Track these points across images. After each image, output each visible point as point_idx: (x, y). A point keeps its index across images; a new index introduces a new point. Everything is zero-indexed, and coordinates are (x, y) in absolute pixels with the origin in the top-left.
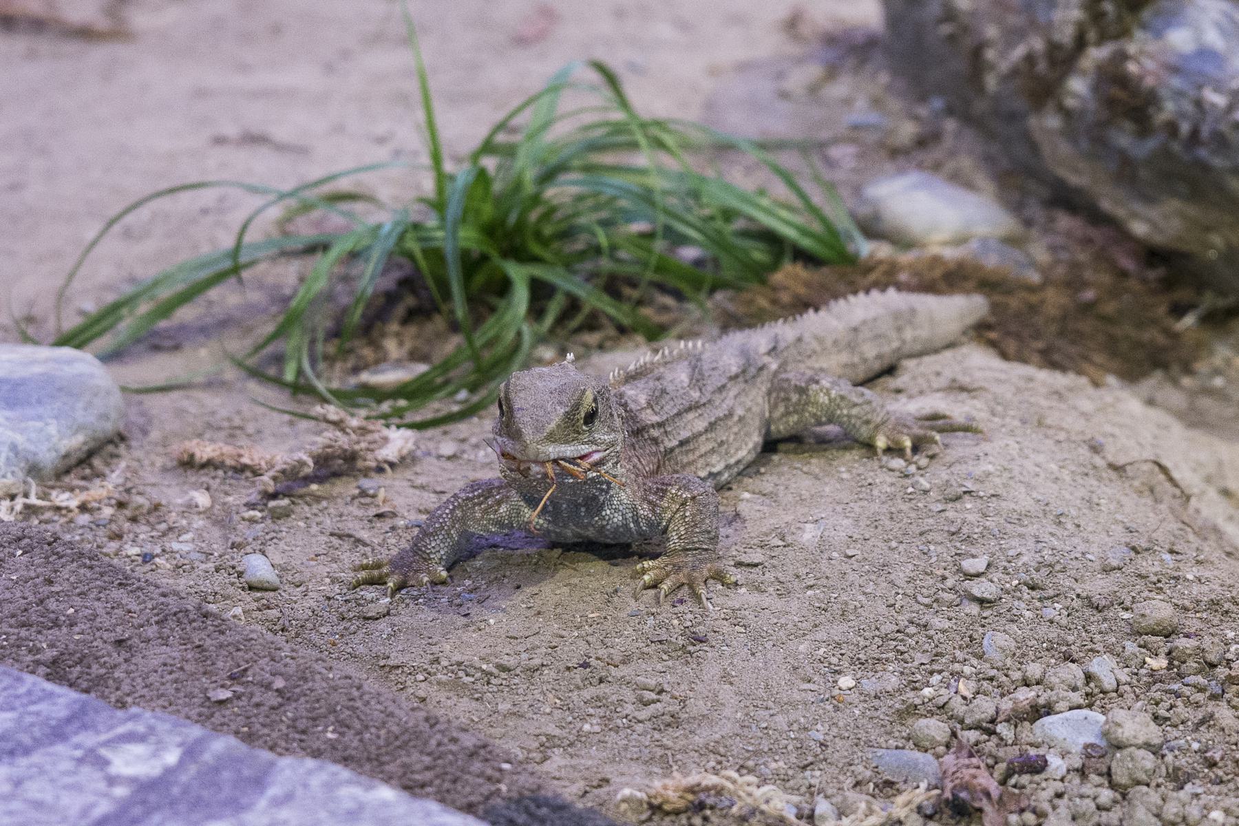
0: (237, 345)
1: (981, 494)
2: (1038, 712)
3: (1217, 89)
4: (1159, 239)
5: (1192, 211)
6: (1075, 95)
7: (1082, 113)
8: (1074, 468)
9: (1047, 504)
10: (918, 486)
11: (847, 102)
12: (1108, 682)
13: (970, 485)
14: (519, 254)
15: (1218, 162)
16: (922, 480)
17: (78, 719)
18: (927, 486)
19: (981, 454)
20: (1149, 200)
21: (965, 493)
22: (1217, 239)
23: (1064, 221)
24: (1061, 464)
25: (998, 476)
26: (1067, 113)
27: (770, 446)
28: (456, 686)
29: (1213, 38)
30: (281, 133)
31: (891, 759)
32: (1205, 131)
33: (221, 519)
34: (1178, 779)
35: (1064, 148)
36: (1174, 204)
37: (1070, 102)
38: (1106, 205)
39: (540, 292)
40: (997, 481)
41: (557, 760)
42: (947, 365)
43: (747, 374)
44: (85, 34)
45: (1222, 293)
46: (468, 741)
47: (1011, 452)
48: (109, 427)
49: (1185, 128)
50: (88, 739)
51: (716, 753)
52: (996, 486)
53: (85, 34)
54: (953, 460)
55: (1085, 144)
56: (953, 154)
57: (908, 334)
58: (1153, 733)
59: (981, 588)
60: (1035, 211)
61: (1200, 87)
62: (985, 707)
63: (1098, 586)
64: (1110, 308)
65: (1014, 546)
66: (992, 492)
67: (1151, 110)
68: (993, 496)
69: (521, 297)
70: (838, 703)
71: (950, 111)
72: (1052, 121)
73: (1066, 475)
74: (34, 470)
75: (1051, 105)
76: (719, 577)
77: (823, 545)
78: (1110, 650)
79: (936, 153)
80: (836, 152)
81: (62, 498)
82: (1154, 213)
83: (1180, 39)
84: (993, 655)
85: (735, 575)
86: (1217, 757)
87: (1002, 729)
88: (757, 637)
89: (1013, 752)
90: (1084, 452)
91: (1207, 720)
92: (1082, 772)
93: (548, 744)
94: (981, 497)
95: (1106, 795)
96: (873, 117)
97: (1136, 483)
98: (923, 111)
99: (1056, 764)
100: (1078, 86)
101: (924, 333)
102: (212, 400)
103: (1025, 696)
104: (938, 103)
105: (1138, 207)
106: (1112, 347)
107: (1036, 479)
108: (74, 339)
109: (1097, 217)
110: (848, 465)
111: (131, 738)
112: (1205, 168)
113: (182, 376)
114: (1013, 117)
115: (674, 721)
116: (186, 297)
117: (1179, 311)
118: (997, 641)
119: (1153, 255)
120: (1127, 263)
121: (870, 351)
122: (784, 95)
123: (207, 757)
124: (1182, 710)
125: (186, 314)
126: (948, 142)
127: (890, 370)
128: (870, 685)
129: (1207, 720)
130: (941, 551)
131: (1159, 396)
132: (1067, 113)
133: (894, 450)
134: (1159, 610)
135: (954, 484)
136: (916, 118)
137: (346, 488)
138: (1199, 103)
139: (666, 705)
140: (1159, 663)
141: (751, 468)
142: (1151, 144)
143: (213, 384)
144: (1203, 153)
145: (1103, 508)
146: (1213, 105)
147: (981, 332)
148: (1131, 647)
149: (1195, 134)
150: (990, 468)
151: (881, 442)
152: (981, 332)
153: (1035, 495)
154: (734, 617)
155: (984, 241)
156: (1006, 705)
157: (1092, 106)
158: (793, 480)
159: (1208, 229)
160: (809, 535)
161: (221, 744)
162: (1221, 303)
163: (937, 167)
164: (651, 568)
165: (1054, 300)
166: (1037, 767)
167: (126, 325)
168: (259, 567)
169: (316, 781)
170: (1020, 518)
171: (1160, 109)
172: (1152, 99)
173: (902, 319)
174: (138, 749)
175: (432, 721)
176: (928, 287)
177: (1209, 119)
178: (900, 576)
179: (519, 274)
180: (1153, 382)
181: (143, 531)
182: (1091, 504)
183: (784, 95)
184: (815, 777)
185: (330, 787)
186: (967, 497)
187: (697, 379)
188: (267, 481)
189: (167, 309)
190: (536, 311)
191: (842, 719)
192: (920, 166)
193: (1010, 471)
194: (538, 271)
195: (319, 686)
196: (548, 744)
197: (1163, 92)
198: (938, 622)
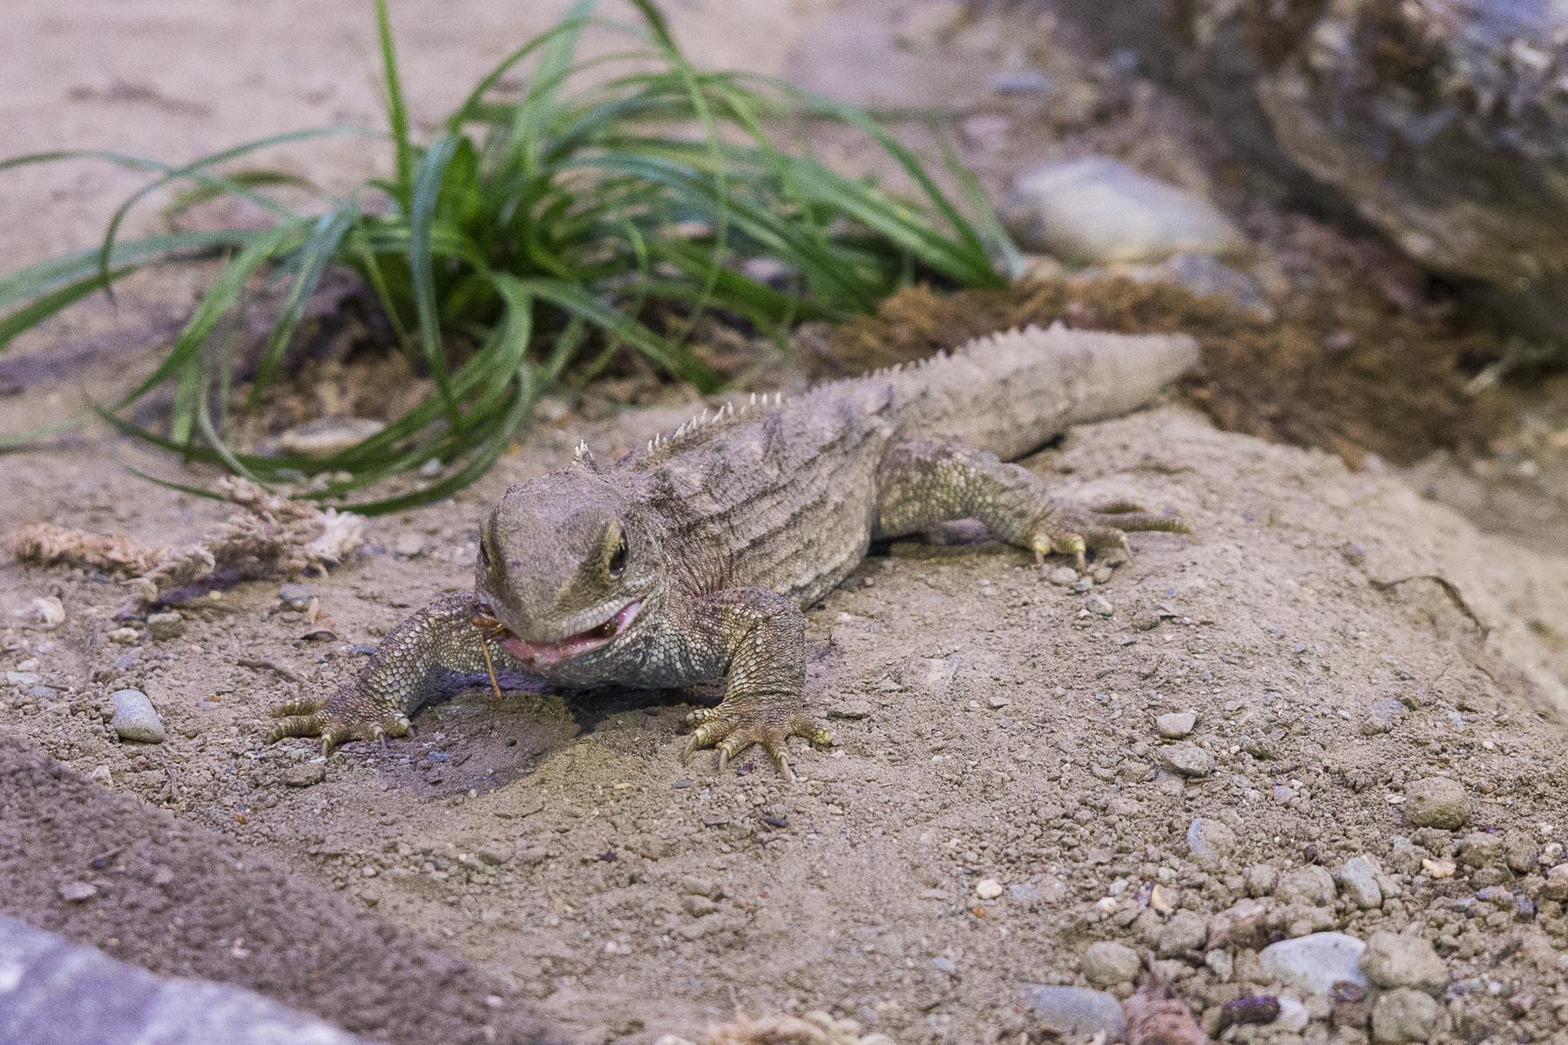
0: (105, 389)
1: (1187, 620)
2: (1266, 935)
3: (1534, 44)
4: (1445, 260)
5: (1494, 220)
6: (1327, 50)
7: (1337, 75)
8: (1321, 586)
9: (1282, 637)
11: (994, 55)
12: (1370, 895)
14: (523, 268)
15: (1533, 150)
18: (1109, 608)
19: (1187, 564)
20: (1432, 203)
21: (1163, 618)
22: (1528, 261)
23: (1308, 233)
24: (1303, 579)
25: (1212, 595)
26: (1314, 76)
27: (880, 547)
28: (420, 884)
30: (171, 85)
32: (1516, 103)
33: (80, 641)
35: (1310, 127)
36: (1469, 209)
37: (1320, 60)
39: (547, 319)
40: (1211, 601)
41: (568, 995)
42: (1139, 434)
43: (844, 445)
45: (1534, 340)
46: (439, 964)
47: (1231, 561)
49: (1486, 99)
51: (800, 987)
55: (1339, 121)
56: (1147, 132)
57: (1081, 390)
58: (1434, 968)
62: (1190, 927)
63: (1355, 756)
64: (1372, 358)
65: (1233, 696)
67: (1437, 72)
68: (1204, 623)
69: (519, 326)
70: (977, 918)
71: (1143, 71)
73: (1308, 595)
76: (807, 733)
77: (957, 690)
79: (1123, 132)
80: (978, 127)
82: (1438, 222)
84: (1203, 852)
85: (830, 732)
87: (1215, 959)
89: (1230, 993)
90: (1335, 562)
91: (1511, 952)
93: (555, 970)
96: (1031, 79)
97: (1411, 610)
98: (1104, 70)
101: (1104, 389)
102: (66, 469)
103: (1248, 911)
104: (1126, 59)
105: (1416, 213)
109: (1355, 227)
112: (1511, 155)
113: (24, 435)
114: (1235, 81)
115: (739, 940)
117: (1471, 364)
120: (1397, 294)
121: (1026, 414)
122: (903, 44)
124: (1475, 936)
125: (29, 343)
126: (1140, 116)
127: (1055, 442)
128: (1023, 893)
129: (1511, 952)
132: (1314, 76)
133: (1061, 556)
134: (1444, 791)
135: (1148, 605)
136: (1093, 80)
137: (262, 597)
138: (1507, 64)
139: (726, 917)
140: (1443, 868)
142: (1436, 122)
144: (1512, 135)
145: (1363, 645)
146: (1528, 67)
148: (1402, 844)
149: (1500, 107)
150: (1201, 583)
151: (1041, 544)
153: (1264, 623)
154: (827, 792)
156: (1221, 924)
157: (1351, 65)
158: (914, 597)
159: (1516, 247)
160: (936, 675)
161: (81, 960)
162: (1533, 354)
163: (1123, 152)
165: (1293, 345)
168: (135, 709)
169: (219, 1016)
170: (1243, 656)
171: (1450, 71)
173: (1073, 369)
175: (387, 934)
178: (1068, 736)
179: (516, 293)
180: (1432, 467)
182: (1346, 637)
183: (903, 44)
186: (1165, 624)
187: (775, 450)
190: (540, 349)
191: (982, 941)
192: (1099, 149)
193: (1230, 587)
194: (545, 290)
195: (223, 880)
197: (1455, 47)
198: (1124, 804)
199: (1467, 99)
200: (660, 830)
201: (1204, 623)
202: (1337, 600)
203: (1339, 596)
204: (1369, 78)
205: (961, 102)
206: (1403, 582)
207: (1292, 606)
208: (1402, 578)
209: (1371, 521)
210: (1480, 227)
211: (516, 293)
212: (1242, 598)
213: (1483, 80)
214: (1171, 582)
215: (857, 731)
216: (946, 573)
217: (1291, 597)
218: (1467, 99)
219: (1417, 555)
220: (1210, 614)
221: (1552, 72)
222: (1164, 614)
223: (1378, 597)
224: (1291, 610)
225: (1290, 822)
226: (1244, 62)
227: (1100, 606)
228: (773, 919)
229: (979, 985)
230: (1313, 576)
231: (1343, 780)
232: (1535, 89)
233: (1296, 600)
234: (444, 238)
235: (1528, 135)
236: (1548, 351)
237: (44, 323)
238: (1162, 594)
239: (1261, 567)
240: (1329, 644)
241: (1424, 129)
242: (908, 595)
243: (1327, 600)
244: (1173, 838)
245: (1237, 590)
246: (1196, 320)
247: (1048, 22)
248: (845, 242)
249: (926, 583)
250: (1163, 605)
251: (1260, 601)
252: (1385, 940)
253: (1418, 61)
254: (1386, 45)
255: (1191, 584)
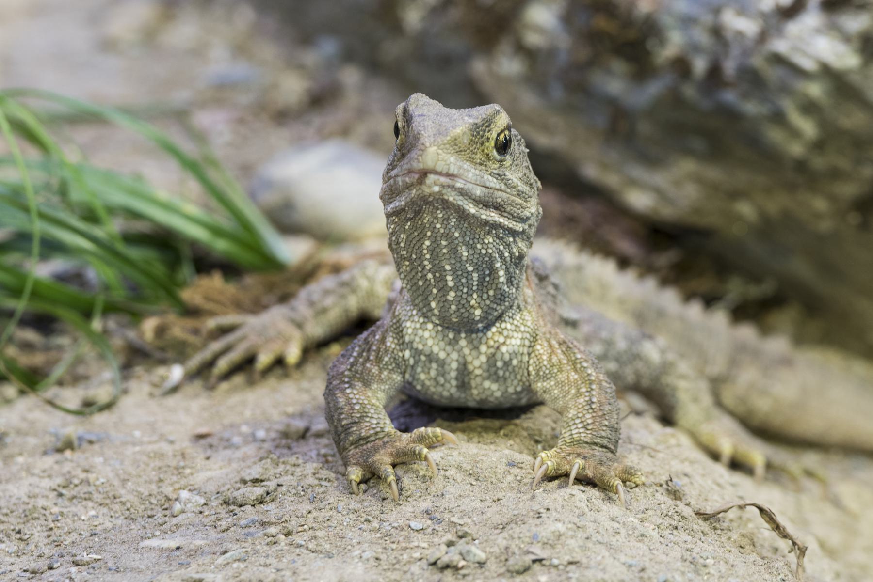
1: (556, 562)
3: (742, 11)
4: (667, 212)
5: (713, 173)
6: (539, 30)
7: (551, 53)
8: (659, 521)
9: (643, 570)
10: (471, 558)
11: (198, 52)
13: (541, 553)
15: (752, 108)
16: (474, 549)
18: (482, 556)
19: (542, 510)
20: (651, 161)
21: (534, 561)
22: (746, 209)
24: (641, 516)
25: (572, 537)
32: (730, 67)
36: (687, 166)
37: (533, 39)
38: (591, 171)
40: (572, 542)
45: (755, 277)
47: (578, 504)
49: (700, 65)
52: (572, 551)
54: (505, 520)
55: (558, 92)
56: (361, 113)
61: (717, 11)
66: (568, 558)
67: (650, 44)
68: (571, 563)
71: (348, 56)
73: (650, 529)
75: (505, 47)
79: (334, 118)
80: (205, 119)
82: (660, 178)
94: (556, 567)
96: (240, 70)
97: (735, 536)
98: (311, 57)
104: (328, 47)
105: (638, 172)
107: (618, 537)
112: (732, 115)
122: (108, 46)
126: (352, 99)
135: (516, 550)
136: (300, 67)
138: (717, 32)
142: (654, 89)
144: (729, 97)
145: (712, 571)
146: (740, 34)
149: (715, 73)
150: (560, 527)
153: (623, 558)
157: (564, 41)
158: (300, 562)
159: (735, 195)
162: (755, 291)
163: (345, 132)
171: (662, 41)
177: (735, 52)
183: (108, 46)
186: (536, 567)
192: (323, 136)
193: (584, 528)
197: (666, 20)
199: (681, 66)
201: (571, 563)
202: (675, 532)
203: (676, 528)
204: (584, 54)
205: (181, 96)
206: (725, 511)
207: (640, 541)
208: (725, 507)
209: (675, 457)
210: (699, 180)
212: (596, 537)
213: (696, 48)
214: (534, 529)
217: (637, 533)
218: (681, 66)
219: (719, 485)
220: (574, 555)
221: (763, 37)
222: (534, 557)
223: (705, 526)
224: (640, 544)
226: (455, 44)
227: (475, 555)
230: (650, 513)
232: (746, 53)
233: (642, 535)
235: (745, 96)
236: (766, 289)
238: (527, 540)
239: (605, 508)
240: (683, 573)
242: (294, 561)
243: (666, 533)
245: (591, 530)
247: (246, 16)
248: (130, 239)
249: (307, 548)
250: (531, 550)
251: (612, 538)
253: (632, 34)
254: (601, 22)
255: (553, 528)
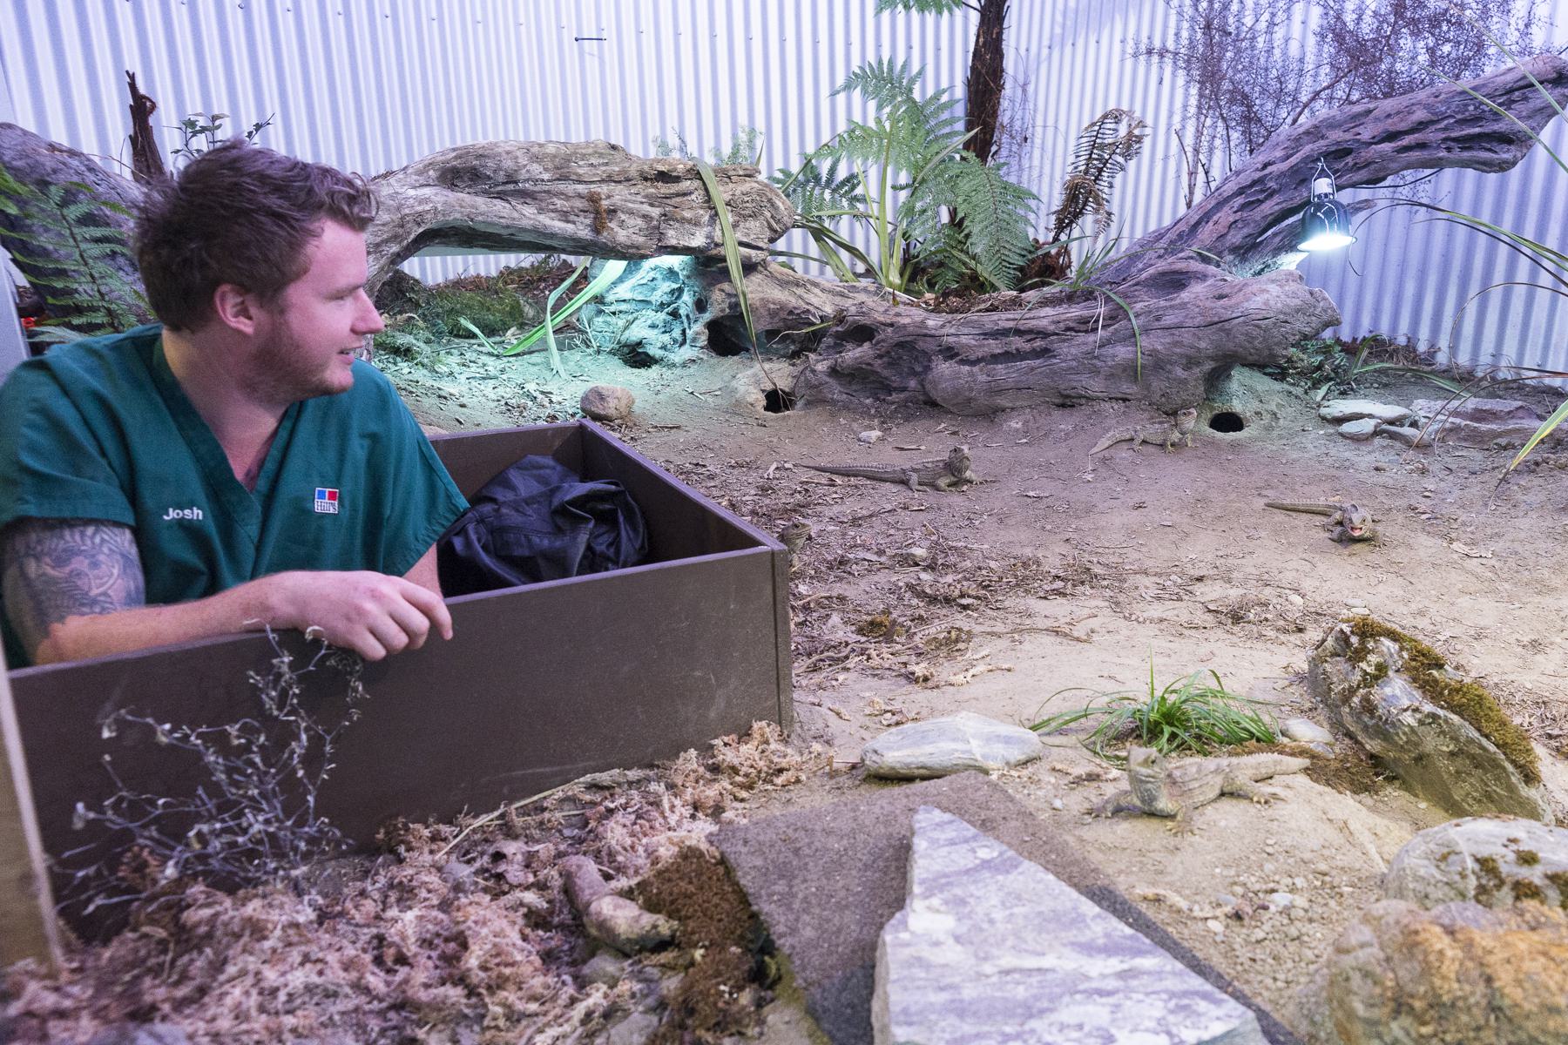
0: (1083, 736)
2: (1273, 891)
12: (1299, 886)
14: (1172, 725)
17: (974, 838)
23: (1347, 741)
26: (1351, 708)
27: (1222, 794)
28: (1100, 850)
29: (1398, 692)
30: (1118, 678)
31: (1224, 896)
33: (1056, 787)
34: (1311, 920)
35: (1349, 718)
39: (1173, 736)
41: (1122, 878)
42: (1288, 779)
43: (1217, 771)
44: (1078, 640)
46: (1093, 866)
48: (1034, 755)
50: (974, 844)
51: (1171, 885)
53: (1078, 640)
57: (1278, 768)
58: (1306, 905)
59: (1269, 850)
60: (1340, 736)
62: (1257, 887)
63: (1307, 856)
64: (1354, 770)
65: (1285, 838)
69: (1166, 736)
70: (1213, 876)
72: (1347, 710)
74: (1008, 763)
76: (1192, 832)
77: (1226, 827)
78: (1305, 877)
81: (1013, 773)
82: (1373, 743)
83: (1388, 691)
84: (1266, 870)
85: (1196, 832)
86: (728, 815)
87: (1261, 895)
88: (1196, 852)
89: (1261, 902)
90: (1320, 813)
91: (1326, 905)
92: (1281, 913)
93: (1120, 872)
95: (1286, 921)
99: (1273, 908)
100: (1356, 700)
101: (1284, 768)
102: (1069, 752)
103: (1272, 885)
106: (1352, 783)
108: (1034, 728)
109: (1357, 742)
110: (1244, 804)
111: (985, 846)
113: (1064, 743)
114: (1337, 706)
115: (1161, 872)
116: (1071, 721)
117: (1377, 775)
118: (1269, 867)
119: (1372, 756)
120: (1363, 757)
121: (1263, 771)
123: (1005, 856)
124: (1320, 899)
125: (1072, 725)
126: (1319, 711)
127: (1271, 778)
128: (1225, 873)
129: (1326, 905)
130: (1262, 836)
131: (1364, 800)
132: (1351, 708)
133: (1259, 802)
134: (1323, 867)
137: (1095, 784)
139: (1161, 867)
140: (1318, 883)
141: (1214, 801)
143: (1073, 747)
147: (1306, 770)
148: (1311, 877)
151: (1255, 799)
152: (1306, 770)
154: (1191, 845)
155: (1319, 743)
156: (1264, 887)
160: (1223, 823)
161: (1011, 853)
164: (1170, 824)
165: (1334, 765)
166: (1266, 908)
167: (1054, 724)
168: (1058, 803)
169: (1032, 870)
170: (1290, 830)
172: (1376, 708)
173: (1276, 763)
174: (986, 850)
175: (1084, 859)
176: (1293, 754)
178: (1246, 841)
179: (1167, 730)
180: (1364, 797)
181: (1033, 786)
182: (1315, 830)
184: (1198, 898)
185: (1036, 872)
187: (1199, 771)
188: (1071, 778)
189: (1067, 722)
190: (1170, 740)
191: (1213, 882)
194: (1175, 730)
195: (1056, 841)
196: (1120, 872)
198: (1253, 857)
200: (1154, 846)
211: (1167, 730)
215: (1202, 833)
216: (1234, 802)
225: (1288, 868)
228: (1170, 869)
229: (1209, 891)
231: (1303, 861)
234: (1154, 716)
237: (191, 647)
241: (1371, 723)
244: (1261, 867)
246: (1313, 756)
252: (1296, 897)
